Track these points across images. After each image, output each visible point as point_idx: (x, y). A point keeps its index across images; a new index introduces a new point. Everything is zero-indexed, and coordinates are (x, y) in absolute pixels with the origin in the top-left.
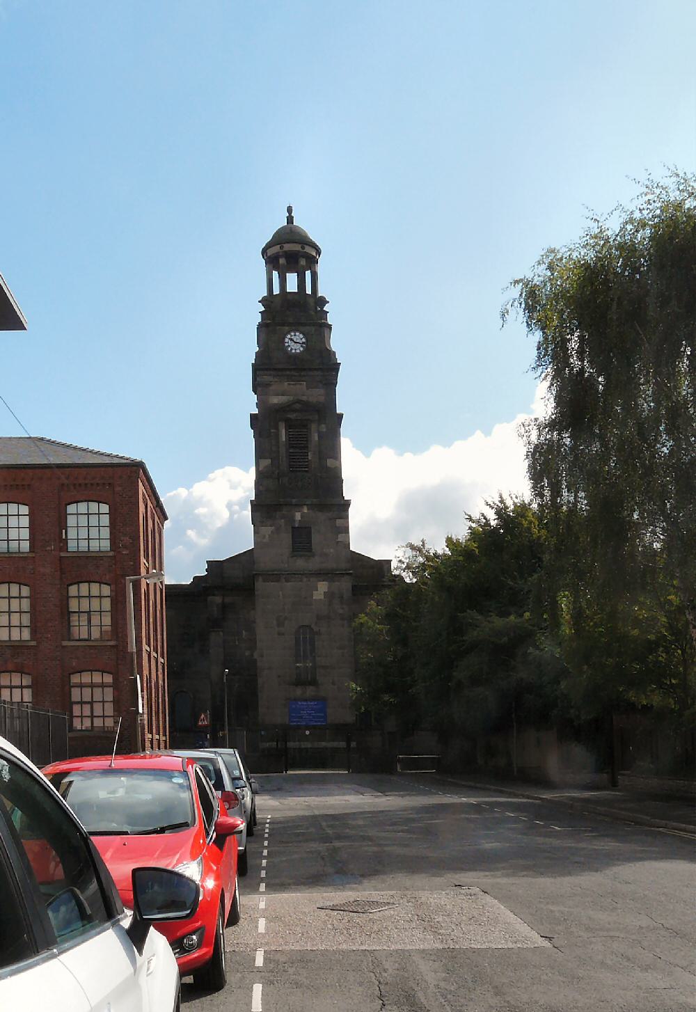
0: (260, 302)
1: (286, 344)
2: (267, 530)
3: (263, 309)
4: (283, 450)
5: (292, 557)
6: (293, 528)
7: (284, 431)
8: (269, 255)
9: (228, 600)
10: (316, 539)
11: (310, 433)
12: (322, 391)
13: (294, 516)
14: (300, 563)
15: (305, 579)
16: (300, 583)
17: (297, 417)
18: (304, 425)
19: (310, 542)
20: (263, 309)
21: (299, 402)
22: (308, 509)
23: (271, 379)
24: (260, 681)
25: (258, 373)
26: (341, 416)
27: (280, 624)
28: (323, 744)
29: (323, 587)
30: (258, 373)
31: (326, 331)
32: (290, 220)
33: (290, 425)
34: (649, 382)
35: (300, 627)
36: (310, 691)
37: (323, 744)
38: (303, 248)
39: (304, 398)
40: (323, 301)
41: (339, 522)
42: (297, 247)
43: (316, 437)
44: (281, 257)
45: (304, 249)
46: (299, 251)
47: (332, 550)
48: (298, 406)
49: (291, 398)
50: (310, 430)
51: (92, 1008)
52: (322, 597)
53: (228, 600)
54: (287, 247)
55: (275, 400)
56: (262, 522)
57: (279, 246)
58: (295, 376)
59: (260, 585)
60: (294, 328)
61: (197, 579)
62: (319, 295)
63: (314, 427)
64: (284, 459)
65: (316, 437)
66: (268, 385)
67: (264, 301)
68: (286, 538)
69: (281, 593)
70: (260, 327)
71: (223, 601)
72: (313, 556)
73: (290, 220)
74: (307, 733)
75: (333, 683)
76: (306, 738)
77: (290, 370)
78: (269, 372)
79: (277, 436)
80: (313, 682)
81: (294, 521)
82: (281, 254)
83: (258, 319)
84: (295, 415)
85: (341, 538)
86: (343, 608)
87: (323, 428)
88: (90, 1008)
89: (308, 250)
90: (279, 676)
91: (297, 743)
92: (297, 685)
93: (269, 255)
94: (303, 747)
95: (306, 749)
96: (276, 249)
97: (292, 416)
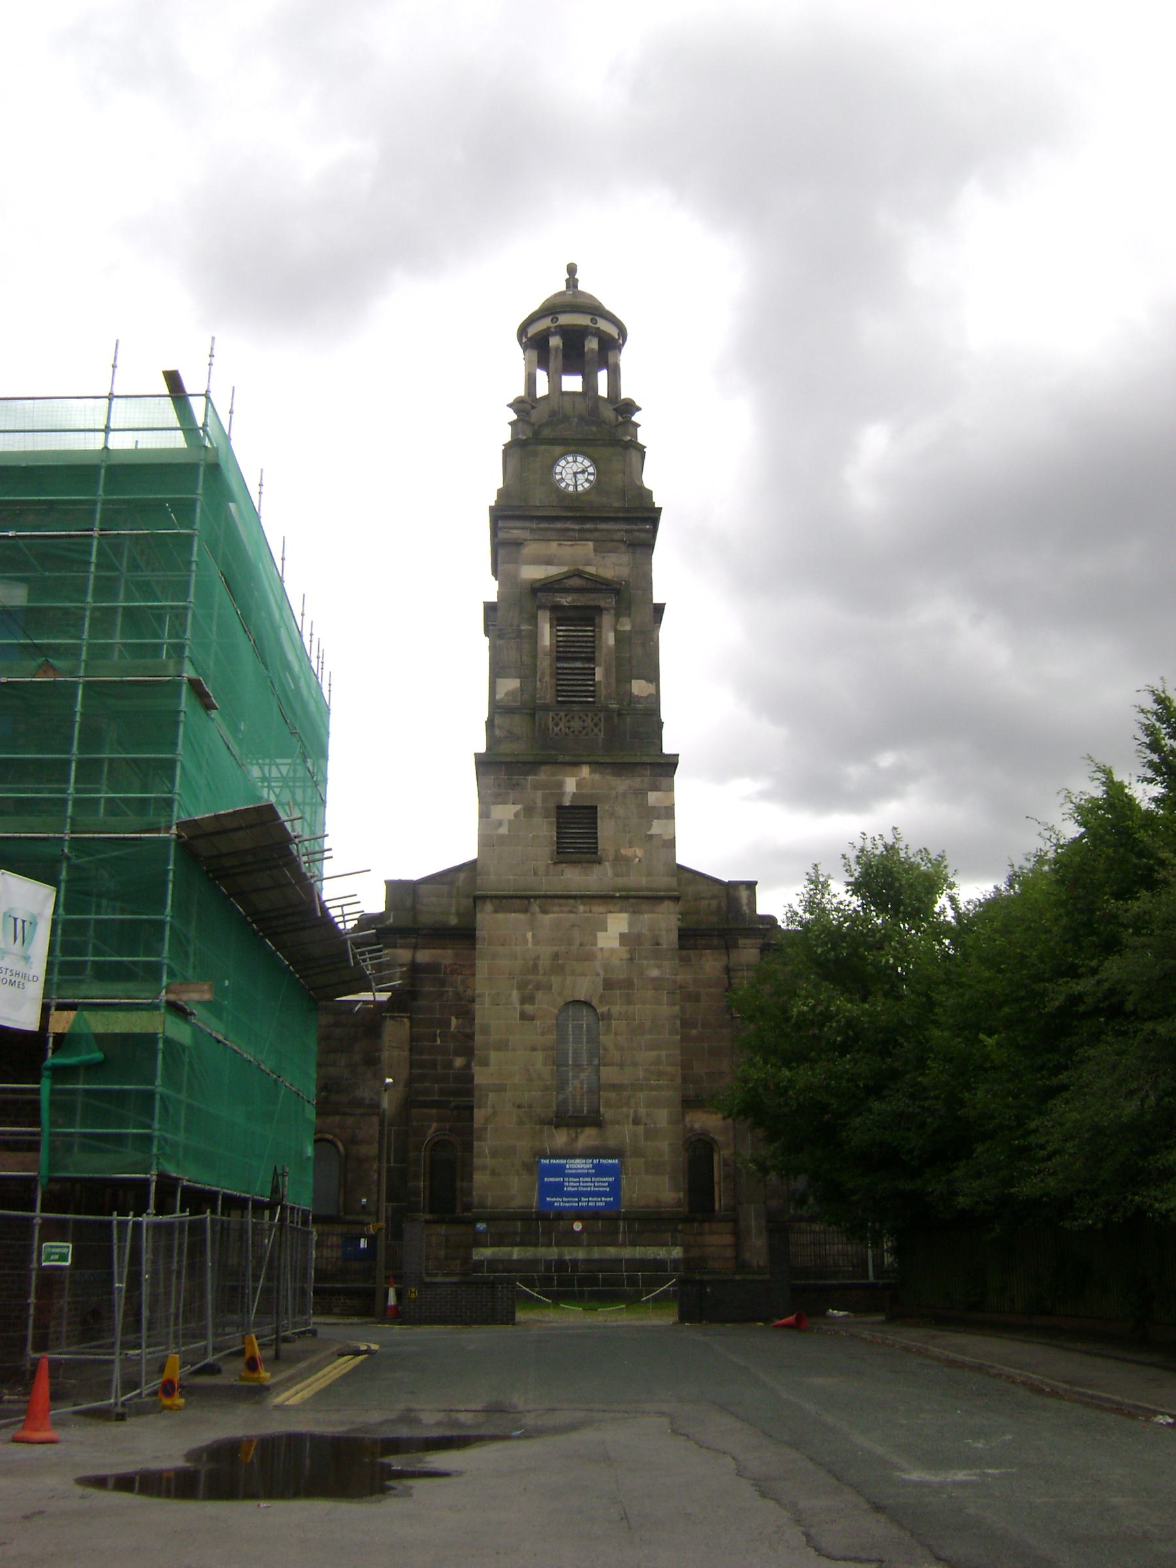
0: (510, 406)
1: (558, 477)
2: (505, 812)
3: (514, 417)
4: (545, 664)
5: (555, 863)
6: (560, 808)
7: (547, 627)
8: (529, 336)
9: (424, 956)
10: (606, 830)
11: (600, 632)
12: (625, 558)
13: (560, 785)
14: (574, 878)
15: (581, 908)
16: (572, 915)
17: (574, 600)
18: (588, 616)
19: (594, 836)
20: (514, 417)
21: (578, 574)
22: (591, 772)
23: (524, 534)
24: (479, 1115)
25: (500, 524)
26: (659, 609)
27: (527, 999)
28: (611, 1252)
29: (618, 924)
30: (500, 524)
31: (634, 454)
32: (572, 282)
33: (561, 616)
34: (909, 886)
35: (567, 1004)
36: (587, 1137)
37: (611, 1252)
38: (594, 321)
39: (591, 570)
40: (629, 408)
41: (653, 798)
42: (583, 320)
43: (610, 639)
44: (554, 334)
45: (596, 323)
46: (586, 327)
47: (639, 852)
48: (576, 582)
49: (565, 569)
50: (600, 627)
51: (182, 430)
52: (616, 944)
53: (424, 956)
54: (565, 319)
55: (533, 573)
56: (497, 795)
57: (550, 318)
58: (573, 530)
59: (488, 920)
60: (572, 448)
61: (500, 492)
62: (622, 398)
63: (607, 620)
64: (547, 678)
65: (610, 639)
66: (518, 544)
67: (518, 405)
68: (545, 830)
69: (529, 935)
70: (508, 450)
71: (414, 957)
72: (599, 862)
73: (572, 282)
74: (578, 1226)
75: (636, 1121)
76: (572, 1239)
77: (566, 519)
78: (527, 524)
79: (534, 636)
80: (595, 1120)
81: (562, 794)
82: (553, 330)
83: (506, 435)
84: (569, 599)
85: (656, 828)
86: (659, 967)
87: (626, 626)
88: (170, 398)
89: (603, 325)
90: (519, 1107)
91: (555, 1249)
92: (557, 1126)
93: (529, 336)
94: (567, 1257)
95: (574, 1262)
96: (545, 323)
97: (566, 600)
